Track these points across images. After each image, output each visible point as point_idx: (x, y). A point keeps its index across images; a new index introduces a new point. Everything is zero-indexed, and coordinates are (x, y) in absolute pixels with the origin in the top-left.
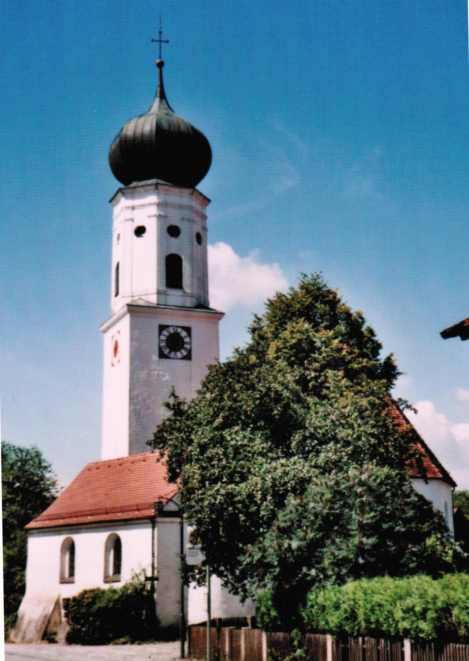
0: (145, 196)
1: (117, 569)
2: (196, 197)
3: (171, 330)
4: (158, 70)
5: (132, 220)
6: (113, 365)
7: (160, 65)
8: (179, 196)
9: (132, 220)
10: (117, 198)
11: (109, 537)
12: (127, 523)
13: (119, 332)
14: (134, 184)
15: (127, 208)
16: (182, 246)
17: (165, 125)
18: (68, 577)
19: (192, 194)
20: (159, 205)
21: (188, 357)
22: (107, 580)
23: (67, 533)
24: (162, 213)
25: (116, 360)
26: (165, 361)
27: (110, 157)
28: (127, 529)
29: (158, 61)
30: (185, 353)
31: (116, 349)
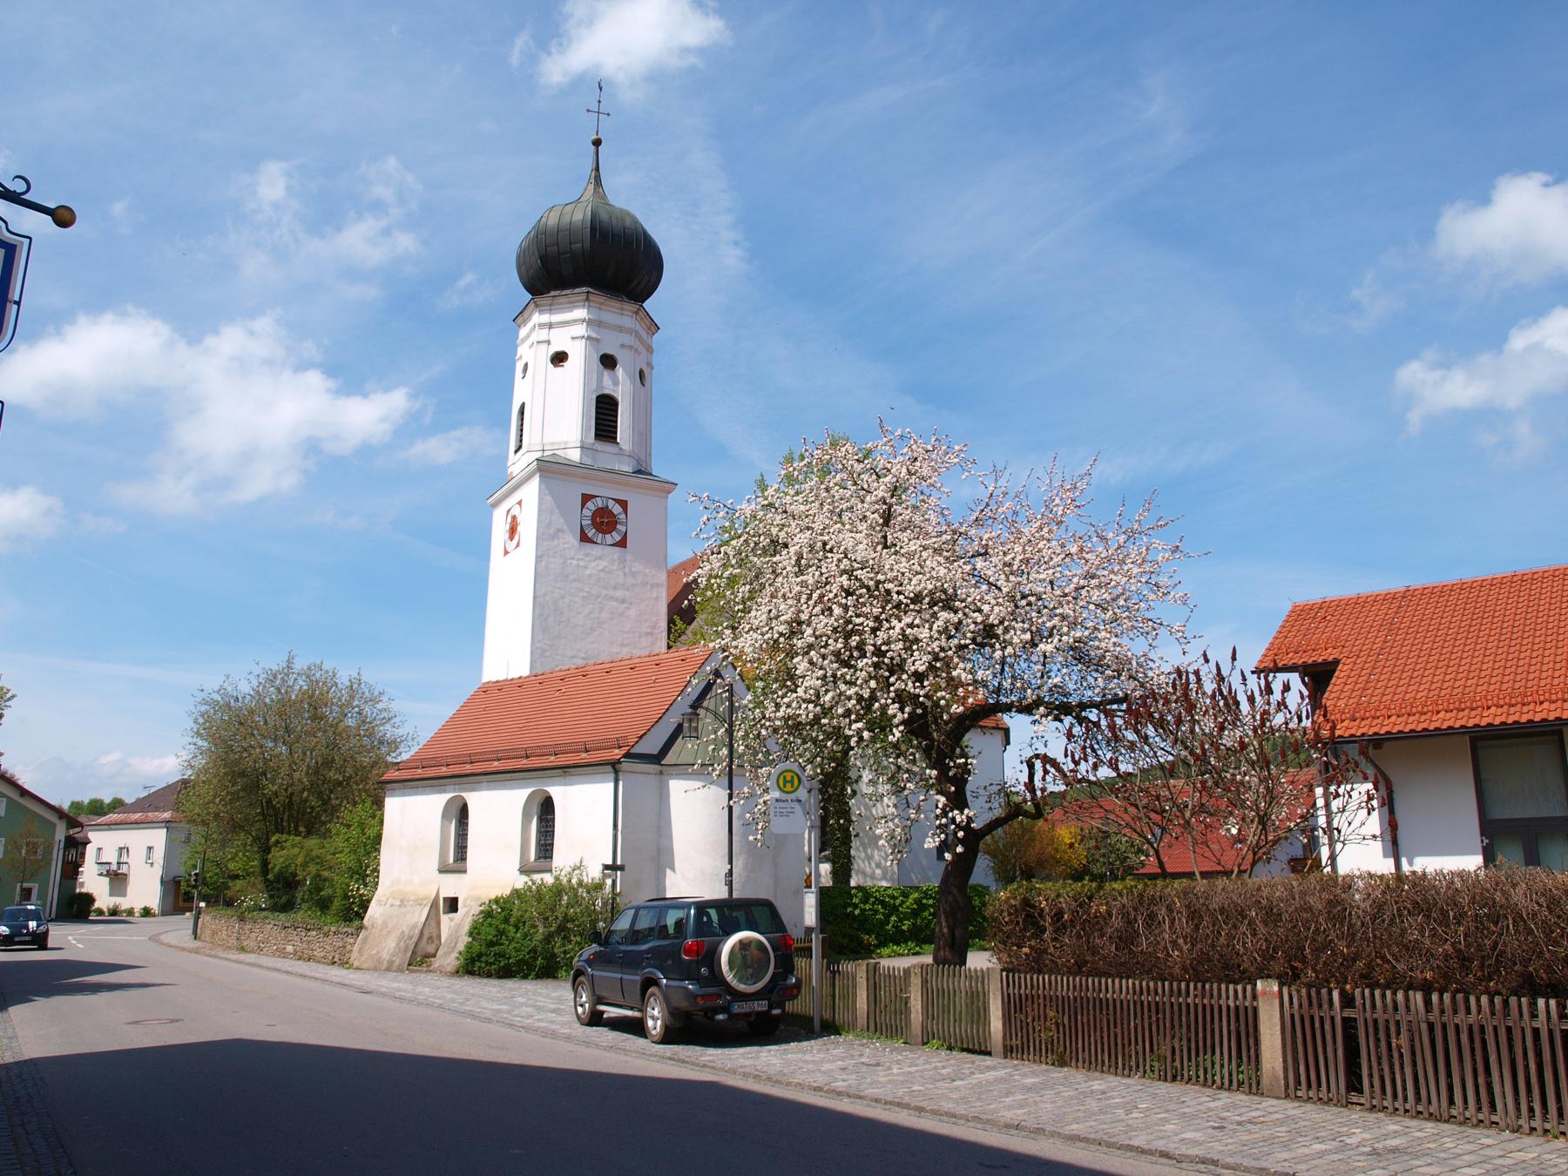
0: (570, 309)
1: (546, 849)
2: (642, 319)
3: (600, 503)
4: (593, 148)
5: (548, 342)
6: (506, 553)
7: (597, 143)
8: (619, 314)
9: (548, 342)
10: (526, 314)
11: (449, 802)
12: (567, 771)
13: (520, 503)
14: (553, 293)
15: (541, 326)
16: (621, 386)
17: (604, 216)
18: (458, 858)
19: (636, 313)
20: (590, 323)
21: (622, 543)
22: (525, 870)
23: (454, 791)
24: (594, 335)
25: (511, 545)
26: (588, 547)
27: (518, 257)
28: (565, 784)
29: (595, 137)
30: (618, 538)
31: (513, 531)
